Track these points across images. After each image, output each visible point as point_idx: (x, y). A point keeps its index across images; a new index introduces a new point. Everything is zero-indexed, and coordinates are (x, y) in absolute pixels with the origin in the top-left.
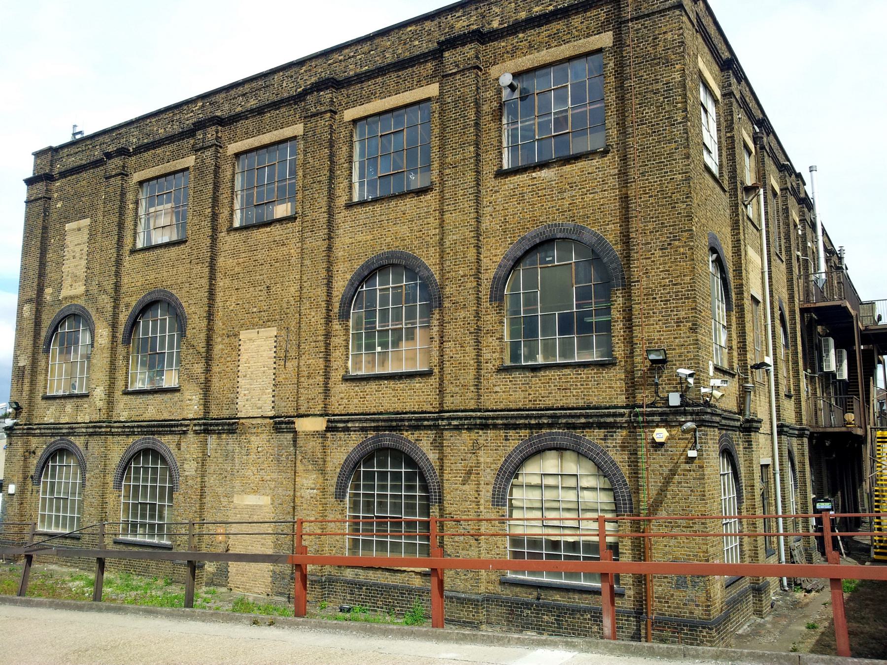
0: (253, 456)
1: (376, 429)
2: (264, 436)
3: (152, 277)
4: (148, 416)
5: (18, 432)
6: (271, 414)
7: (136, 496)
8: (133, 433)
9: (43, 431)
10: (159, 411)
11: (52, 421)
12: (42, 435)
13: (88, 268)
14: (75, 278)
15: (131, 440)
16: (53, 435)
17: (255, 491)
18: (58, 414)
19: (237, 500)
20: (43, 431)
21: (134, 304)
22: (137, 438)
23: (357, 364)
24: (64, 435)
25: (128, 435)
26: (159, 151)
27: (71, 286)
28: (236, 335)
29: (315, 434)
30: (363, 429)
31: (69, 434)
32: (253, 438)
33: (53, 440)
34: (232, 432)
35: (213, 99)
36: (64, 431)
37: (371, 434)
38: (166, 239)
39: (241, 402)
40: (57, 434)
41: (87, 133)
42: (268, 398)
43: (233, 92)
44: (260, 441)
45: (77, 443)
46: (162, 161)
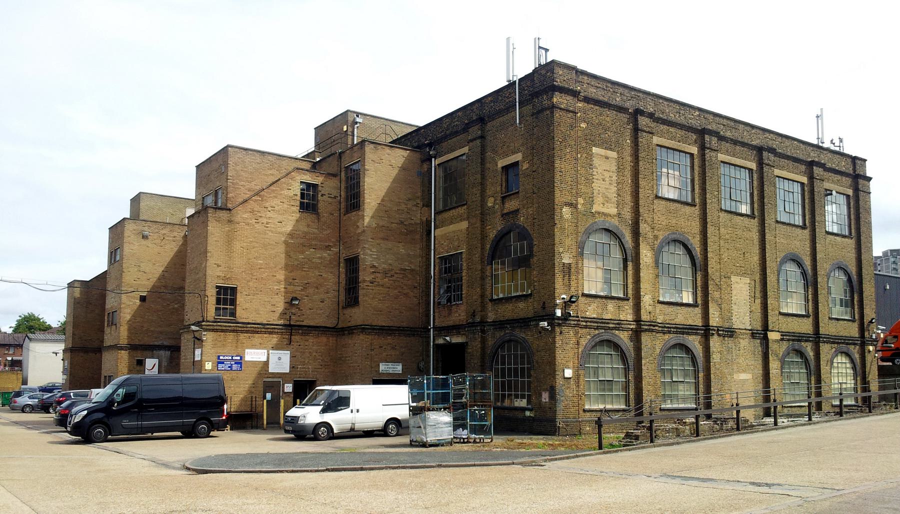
0: (742, 351)
1: (793, 340)
2: (759, 341)
3: (674, 221)
4: (677, 321)
5: (572, 322)
6: (750, 328)
7: (503, 376)
8: (669, 332)
9: (589, 324)
10: (686, 319)
11: (595, 316)
12: (586, 327)
13: (619, 195)
14: (607, 200)
15: (667, 337)
16: (597, 328)
17: (744, 371)
18: (600, 311)
19: (735, 376)
20: (589, 324)
21: (661, 237)
22: (671, 336)
23: (664, 296)
24: (609, 328)
25: (664, 333)
26: (672, 130)
27: (603, 204)
28: (729, 278)
29: (777, 341)
30: (788, 340)
31: (615, 328)
32: (741, 341)
33: (597, 332)
34: (731, 336)
35: (706, 116)
36: (611, 326)
37: (791, 343)
38: (671, 196)
39: (734, 319)
40: (602, 328)
41: (846, 151)
42: (747, 319)
43: (717, 119)
44: (745, 343)
45: (622, 336)
46: (672, 138)
